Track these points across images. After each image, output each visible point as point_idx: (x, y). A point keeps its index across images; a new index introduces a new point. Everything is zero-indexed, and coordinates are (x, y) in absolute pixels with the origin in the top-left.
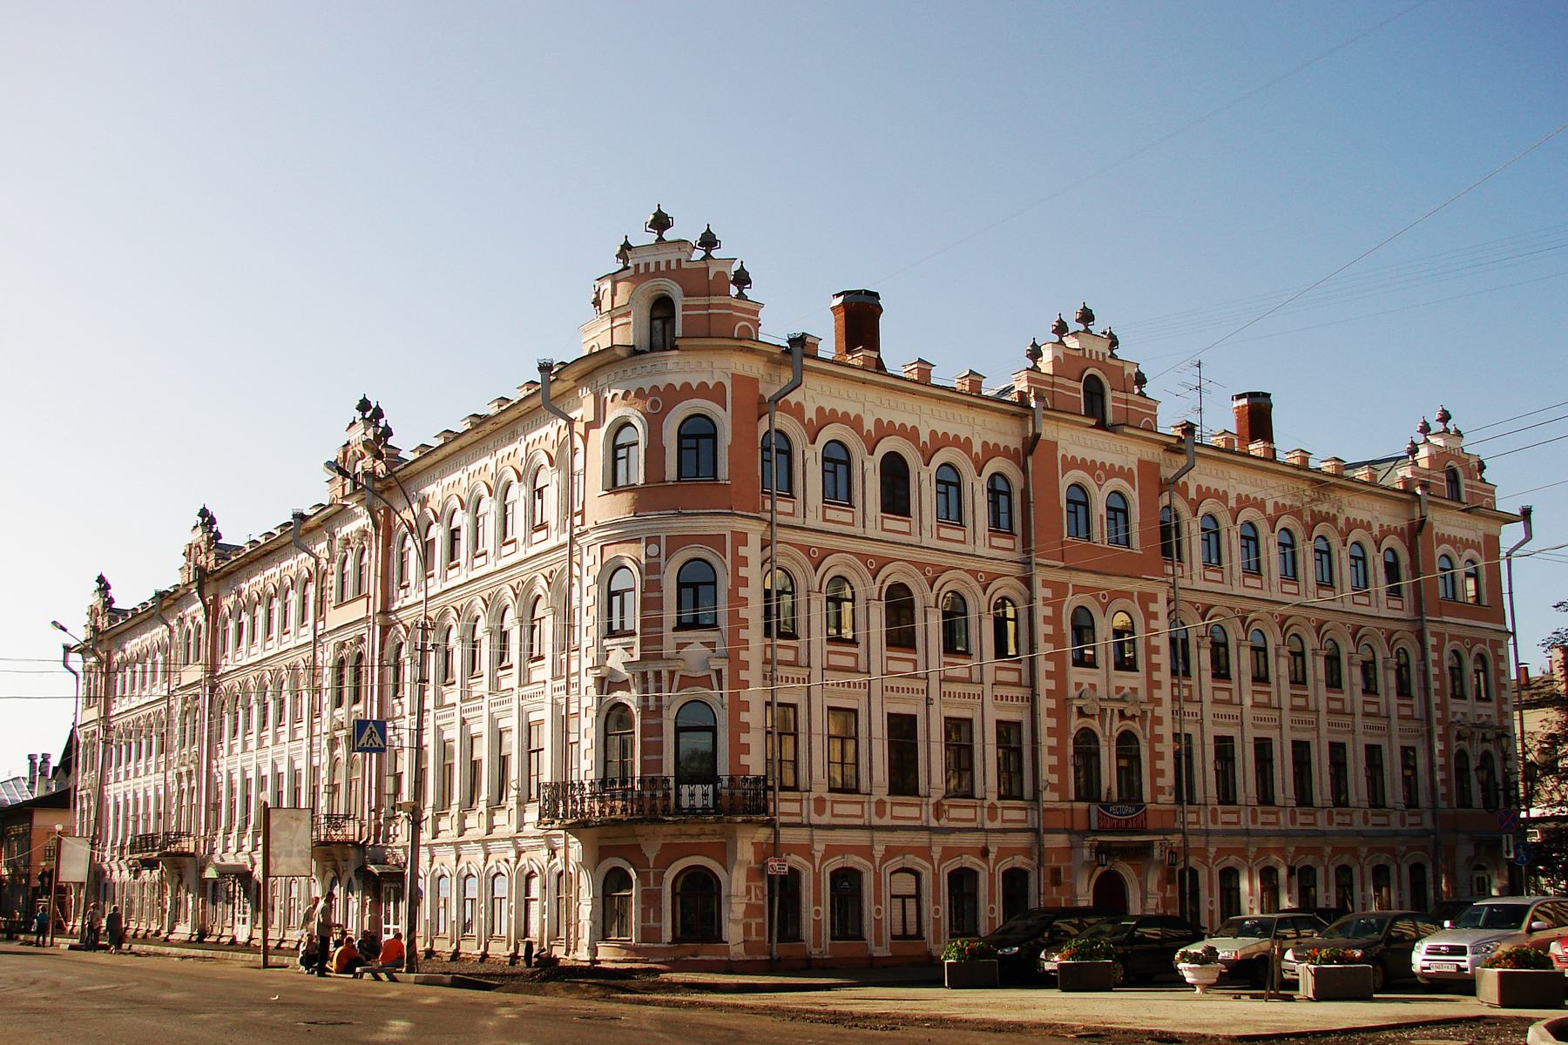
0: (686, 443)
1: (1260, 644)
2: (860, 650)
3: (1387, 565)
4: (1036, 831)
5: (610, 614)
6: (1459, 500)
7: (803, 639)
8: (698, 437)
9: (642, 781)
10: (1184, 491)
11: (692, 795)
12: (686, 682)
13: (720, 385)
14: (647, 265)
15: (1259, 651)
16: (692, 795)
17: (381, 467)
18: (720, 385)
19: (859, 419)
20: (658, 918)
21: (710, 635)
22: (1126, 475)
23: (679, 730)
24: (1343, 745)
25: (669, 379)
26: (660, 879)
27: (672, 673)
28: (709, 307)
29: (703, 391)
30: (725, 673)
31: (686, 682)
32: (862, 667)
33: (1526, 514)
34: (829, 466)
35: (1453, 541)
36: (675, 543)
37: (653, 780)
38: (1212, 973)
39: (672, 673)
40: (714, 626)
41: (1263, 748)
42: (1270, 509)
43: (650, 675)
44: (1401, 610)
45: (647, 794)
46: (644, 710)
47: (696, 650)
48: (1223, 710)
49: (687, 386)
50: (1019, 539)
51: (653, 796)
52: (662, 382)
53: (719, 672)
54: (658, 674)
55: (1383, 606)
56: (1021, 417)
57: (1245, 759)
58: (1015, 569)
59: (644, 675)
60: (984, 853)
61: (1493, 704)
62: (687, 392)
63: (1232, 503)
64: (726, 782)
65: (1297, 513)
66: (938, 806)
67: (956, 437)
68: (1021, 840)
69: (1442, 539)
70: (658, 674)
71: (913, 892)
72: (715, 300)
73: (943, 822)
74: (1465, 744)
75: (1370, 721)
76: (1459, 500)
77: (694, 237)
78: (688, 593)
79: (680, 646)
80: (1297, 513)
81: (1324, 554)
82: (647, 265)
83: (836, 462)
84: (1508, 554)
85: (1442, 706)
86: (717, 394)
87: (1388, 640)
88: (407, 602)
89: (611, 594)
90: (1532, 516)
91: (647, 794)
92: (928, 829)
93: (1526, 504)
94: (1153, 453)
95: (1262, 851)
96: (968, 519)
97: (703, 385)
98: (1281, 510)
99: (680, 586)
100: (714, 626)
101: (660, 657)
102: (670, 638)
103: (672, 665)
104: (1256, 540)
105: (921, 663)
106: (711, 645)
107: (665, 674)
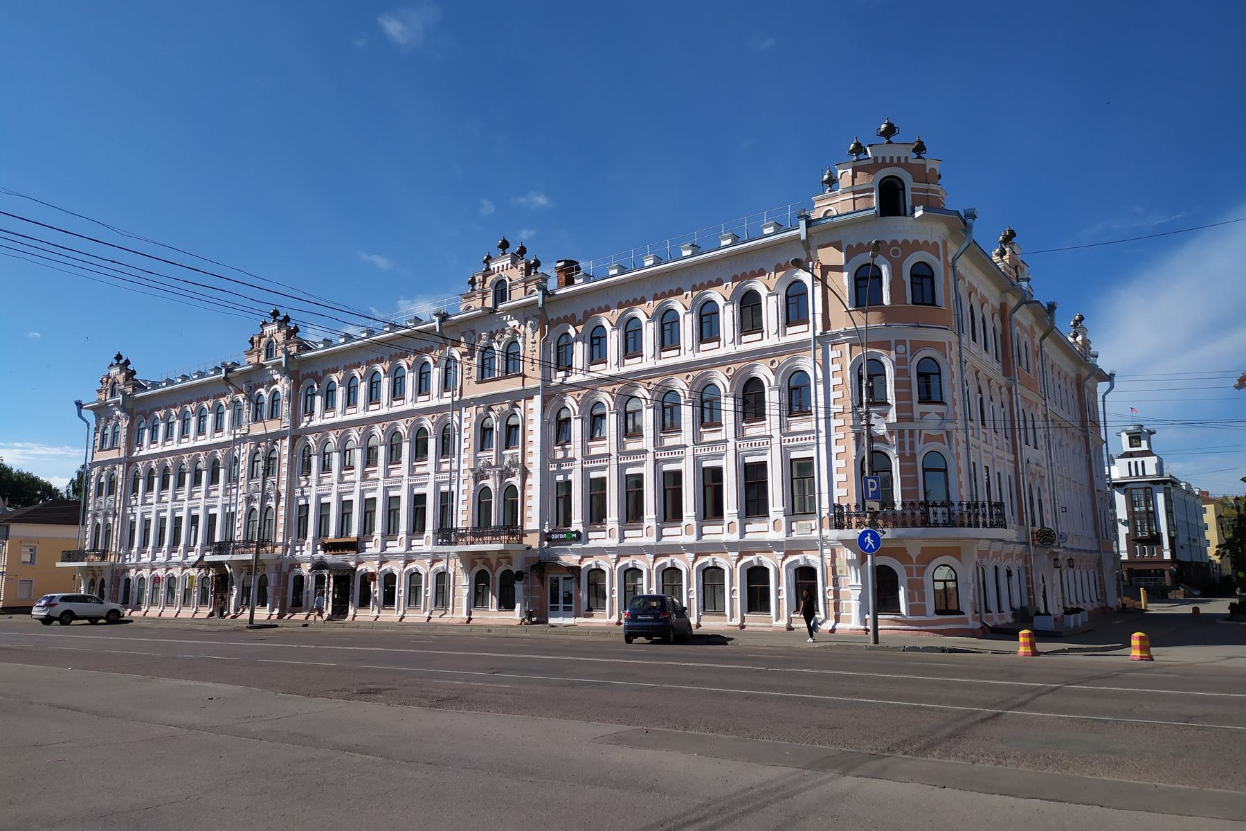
0: (860, 283)
4: (1027, 543)
5: (861, 394)
9: (903, 504)
11: (935, 513)
12: (929, 439)
14: (884, 158)
16: (935, 513)
17: (538, 296)
20: (922, 598)
21: (940, 408)
23: (924, 470)
28: (927, 191)
29: (925, 246)
31: (929, 439)
34: (918, 280)
36: (916, 346)
37: (912, 504)
43: (907, 433)
45: (908, 513)
49: (916, 242)
51: (913, 514)
54: (912, 432)
71: (950, 608)
72: (932, 186)
79: (923, 414)
82: (884, 158)
83: (922, 277)
86: (933, 248)
88: (141, 453)
89: (626, 413)
91: (908, 513)
97: (926, 242)
100: (941, 402)
101: (911, 419)
103: (922, 426)
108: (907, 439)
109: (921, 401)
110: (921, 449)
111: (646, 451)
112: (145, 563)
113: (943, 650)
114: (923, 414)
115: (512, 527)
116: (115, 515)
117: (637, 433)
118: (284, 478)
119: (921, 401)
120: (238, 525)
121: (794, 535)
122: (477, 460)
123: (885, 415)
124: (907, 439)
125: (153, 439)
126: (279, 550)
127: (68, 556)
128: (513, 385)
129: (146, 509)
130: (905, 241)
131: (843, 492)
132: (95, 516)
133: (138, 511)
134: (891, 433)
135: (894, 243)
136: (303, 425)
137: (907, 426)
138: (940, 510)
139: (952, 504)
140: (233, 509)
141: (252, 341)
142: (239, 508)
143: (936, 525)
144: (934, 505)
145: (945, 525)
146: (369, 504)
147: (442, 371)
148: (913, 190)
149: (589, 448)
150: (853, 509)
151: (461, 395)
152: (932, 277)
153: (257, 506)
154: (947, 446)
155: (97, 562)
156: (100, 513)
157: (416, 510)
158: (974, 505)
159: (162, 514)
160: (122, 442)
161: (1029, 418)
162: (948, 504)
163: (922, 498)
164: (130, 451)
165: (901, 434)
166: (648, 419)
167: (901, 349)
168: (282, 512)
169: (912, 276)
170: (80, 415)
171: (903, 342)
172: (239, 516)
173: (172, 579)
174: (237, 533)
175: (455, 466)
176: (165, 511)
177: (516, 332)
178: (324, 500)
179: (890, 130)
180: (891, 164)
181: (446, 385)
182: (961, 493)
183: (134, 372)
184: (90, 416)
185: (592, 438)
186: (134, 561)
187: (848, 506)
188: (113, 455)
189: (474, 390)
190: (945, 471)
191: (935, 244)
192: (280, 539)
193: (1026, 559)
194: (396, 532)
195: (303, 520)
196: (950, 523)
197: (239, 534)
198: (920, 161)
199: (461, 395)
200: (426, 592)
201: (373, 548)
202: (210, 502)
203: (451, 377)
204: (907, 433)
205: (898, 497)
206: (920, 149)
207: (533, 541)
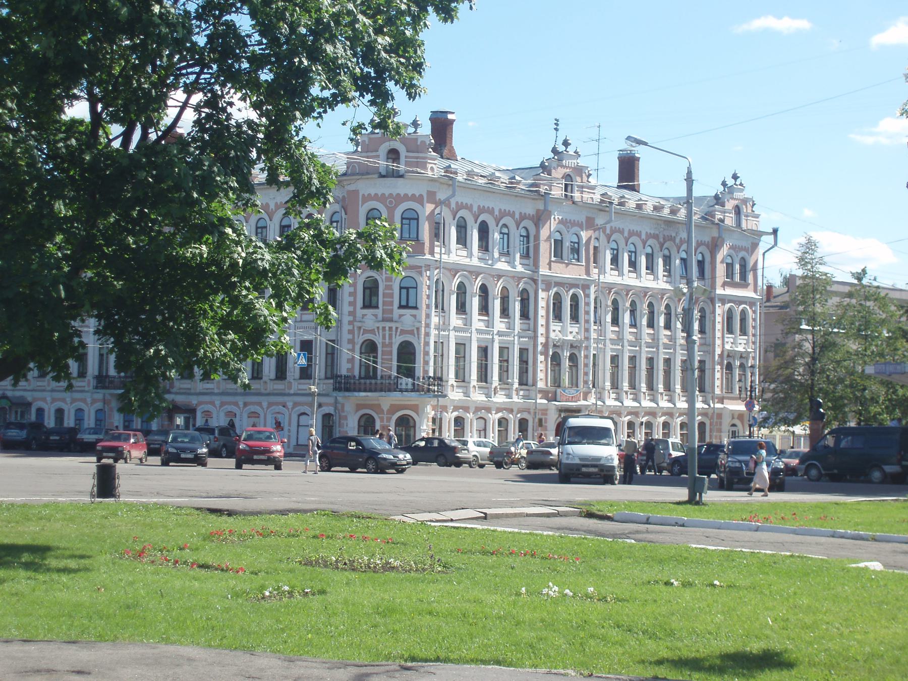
3: (699, 262)
8: (410, 219)
10: (449, 206)
12: (403, 332)
13: (421, 196)
18: (421, 196)
25: (398, 191)
26: (389, 420)
28: (417, 158)
29: (413, 198)
31: (403, 332)
33: (775, 232)
38: (105, 352)
39: (397, 328)
42: (643, 237)
43: (387, 328)
46: (384, 345)
49: (406, 195)
50: (532, 259)
52: (395, 192)
54: (391, 328)
57: (660, 366)
62: (406, 198)
63: (626, 234)
65: (655, 237)
67: (413, 195)
70: (391, 328)
77: (409, 121)
79: (401, 316)
80: (655, 237)
81: (506, 235)
90: (779, 233)
93: (775, 226)
98: (649, 236)
100: (416, 308)
101: (391, 320)
104: (465, 227)
107: (394, 329)
108: (387, 333)
110: (397, 340)
119: (401, 307)
124: (387, 333)
130: (398, 195)
135: (391, 195)
148: (406, 157)
204: (387, 328)
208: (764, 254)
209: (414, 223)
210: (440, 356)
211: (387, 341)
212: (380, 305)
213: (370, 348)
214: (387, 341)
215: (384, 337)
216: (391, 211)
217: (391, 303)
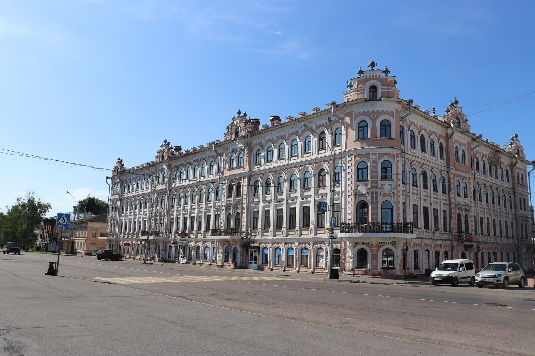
0: (382, 127)
1: (415, 173)
2: (418, 189)
4: (452, 240)
6: (460, 128)
7: (419, 187)
11: (386, 227)
14: (370, 76)
15: (414, 175)
16: (386, 227)
19: (417, 124)
20: (377, 262)
21: (391, 182)
22: (465, 145)
23: (382, 209)
24: (437, 209)
27: (381, 192)
28: (388, 89)
29: (387, 113)
30: (396, 193)
31: (385, 195)
32: (419, 194)
34: (383, 127)
35: (459, 142)
36: (381, 155)
39: (381, 192)
40: (392, 180)
41: (426, 210)
43: (374, 193)
44: (508, 185)
47: (387, 186)
48: (426, 198)
49: (383, 111)
52: (375, 109)
53: (394, 193)
54: (376, 193)
55: (430, 158)
56: (447, 128)
58: (445, 169)
59: (372, 193)
60: (441, 246)
61: (469, 199)
62: (383, 113)
64: (396, 224)
66: (433, 232)
68: (448, 243)
69: (456, 141)
73: (435, 237)
74: (460, 212)
75: (414, 195)
76: (460, 128)
78: (384, 170)
82: (370, 76)
83: (386, 126)
84: (529, 173)
85: (454, 198)
86: (391, 114)
87: (440, 173)
92: (432, 239)
94: (399, 107)
95: (501, 249)
96: (416, 147)
97: (387, 111)
99: (382, 168)
100: (392, 180)
102: (380, 182)
105: (429, 193)
106: (391, 185)
107: (379, 193)
108: (374, 196)
109: (382, 179)
110: (381, 200)
111: (211, 207)
112: (124, 238)
113: (351, 282)
114: (382, 185)
115: (237, 230)
116: (117, 220)
117: (282, 193)
118: (245, 197)
119: (382, 179)
120: (222, 221)
121: (303, 236)
122: (227, 201)
123: (366, 185)
124: (374, 196)
125: (128, 192)
126: (244, 235)
127: (102, 235)
128: (240, 171)
129: (140, 216)
131: (348, 217)
132: (111, 220)
133: (175, 213)
134: (368, 193)
136: (173, 186)
137: (375, 190)
138: (388, 226)
139: (394, 223)
140: (219, 213)
141: (228, 128)
142: (222, 213)
143: (386, 232)
144: (386, 224)
145: (390, 232)
146: (192, 218)
147: (217, 165)
149: (265, 197)
150: (353, 225)
151: (346, 148)
152: (390, 126)
153: (158, 218)
154: (393, 199)
155: (111, 237)
156: (158, 214)
157: (228, 219)
158: (405, 224)
159: (185, 216)
160: (119, 192)
161: (520, 176)
162: (392, 223)
163: (379, 220)
164: (122, 195)
165: (372, 193)
166: (312, 182)
167: (374, 157)
168: (244, 215)
169: (381, 126)
170: (106, 182)
171: (375, 154)
172: (222, 217)
173: (198, 247)
174: (222, 225)
175: (343, 189)
176: (194, 213)
177: (241, 149)
178: (192, 215)
179: (373, 64)
180: (373, 79)
181: (218, 171)
182: (398, 217)
183: (123, 165)
184: (109, 181)
185: (266, 193)
186: (202, 237)
187: (352, 223)
188: (117, 197)
189: (227, 173)
190: (392, 209)
191: (392, 112)
192: (244, 229)
193: (452, 247)
194: (308, 226)
195: (255, 219)
196: (393, 231)
197: (222, 225)
198: (386, 77)
199: (346, 148)
200: (311, 259)
201: (193, 236)
202: (140, 216)
203: (217, 168)
205: (370, 220)
206: (387, 71)
207: (244, 235)
208: (529, 173)
209: (365, 128)
210: (415, 213)
211: (374, 200)
212: (369, 179)
213: (361, 206)
214: (374, 200)
215: (372, 197)
216: (374, 120)
217: (377, 177)
